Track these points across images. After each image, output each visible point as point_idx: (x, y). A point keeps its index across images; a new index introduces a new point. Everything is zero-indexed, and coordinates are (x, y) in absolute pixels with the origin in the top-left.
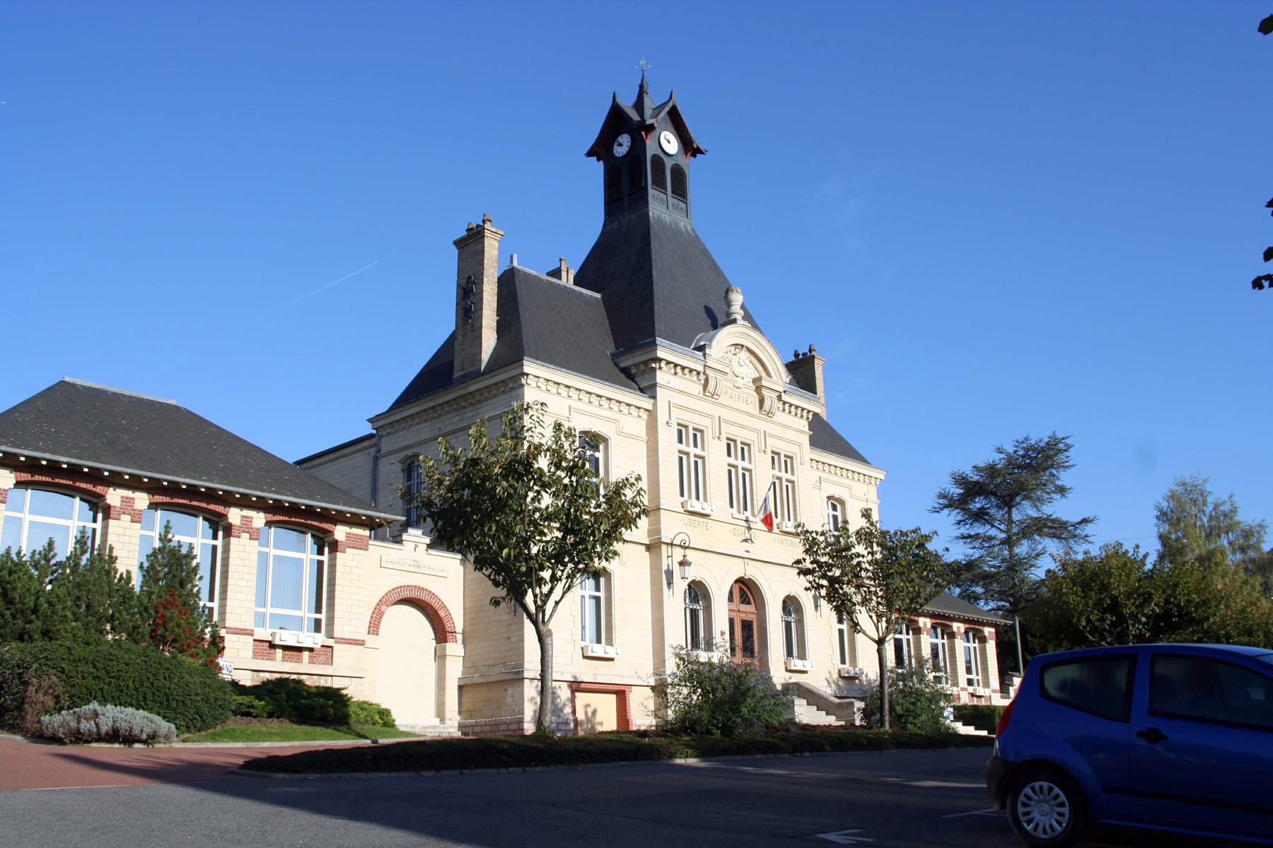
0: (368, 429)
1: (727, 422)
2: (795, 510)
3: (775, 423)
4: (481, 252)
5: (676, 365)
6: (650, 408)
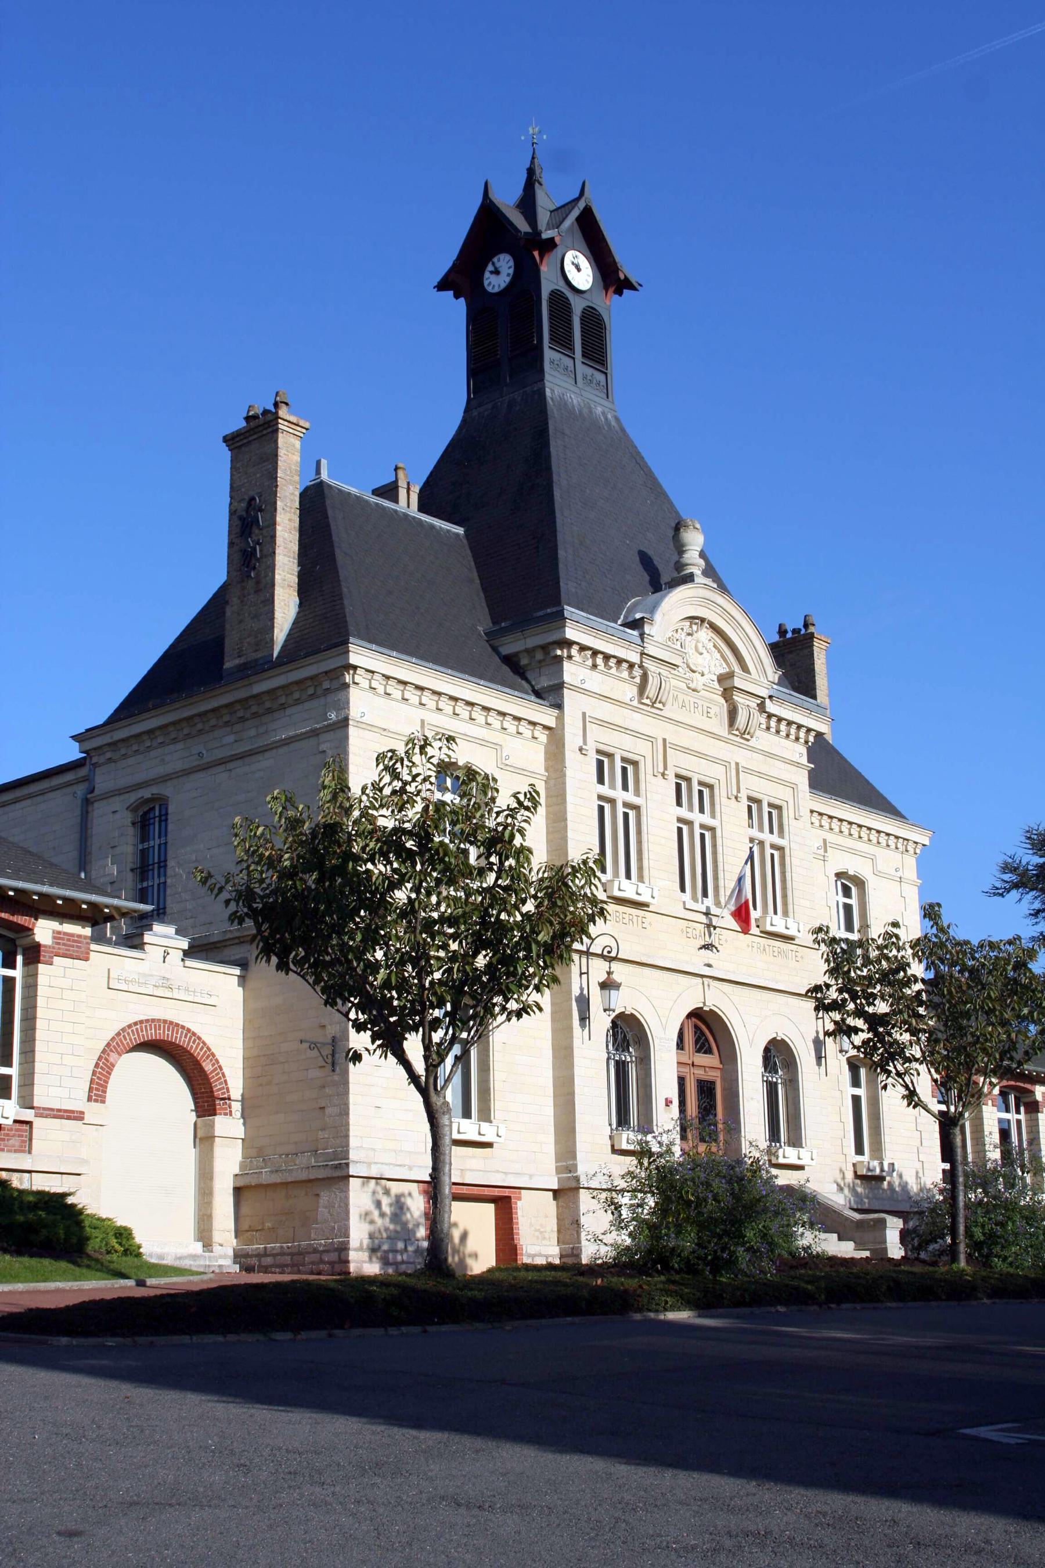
0: (73, 753)
1: (677, 748)
2: (785, 896)
3: (753, 749)
4: (272, 457)
5: (595, 653)
6: (553, 724)
